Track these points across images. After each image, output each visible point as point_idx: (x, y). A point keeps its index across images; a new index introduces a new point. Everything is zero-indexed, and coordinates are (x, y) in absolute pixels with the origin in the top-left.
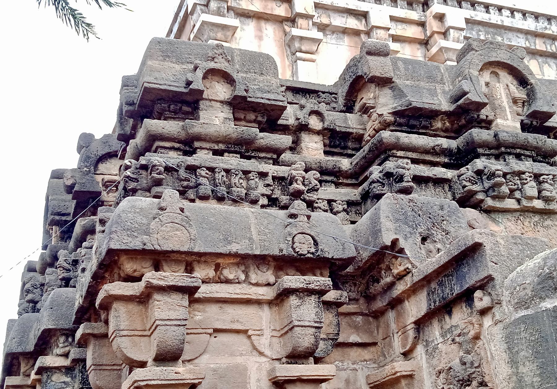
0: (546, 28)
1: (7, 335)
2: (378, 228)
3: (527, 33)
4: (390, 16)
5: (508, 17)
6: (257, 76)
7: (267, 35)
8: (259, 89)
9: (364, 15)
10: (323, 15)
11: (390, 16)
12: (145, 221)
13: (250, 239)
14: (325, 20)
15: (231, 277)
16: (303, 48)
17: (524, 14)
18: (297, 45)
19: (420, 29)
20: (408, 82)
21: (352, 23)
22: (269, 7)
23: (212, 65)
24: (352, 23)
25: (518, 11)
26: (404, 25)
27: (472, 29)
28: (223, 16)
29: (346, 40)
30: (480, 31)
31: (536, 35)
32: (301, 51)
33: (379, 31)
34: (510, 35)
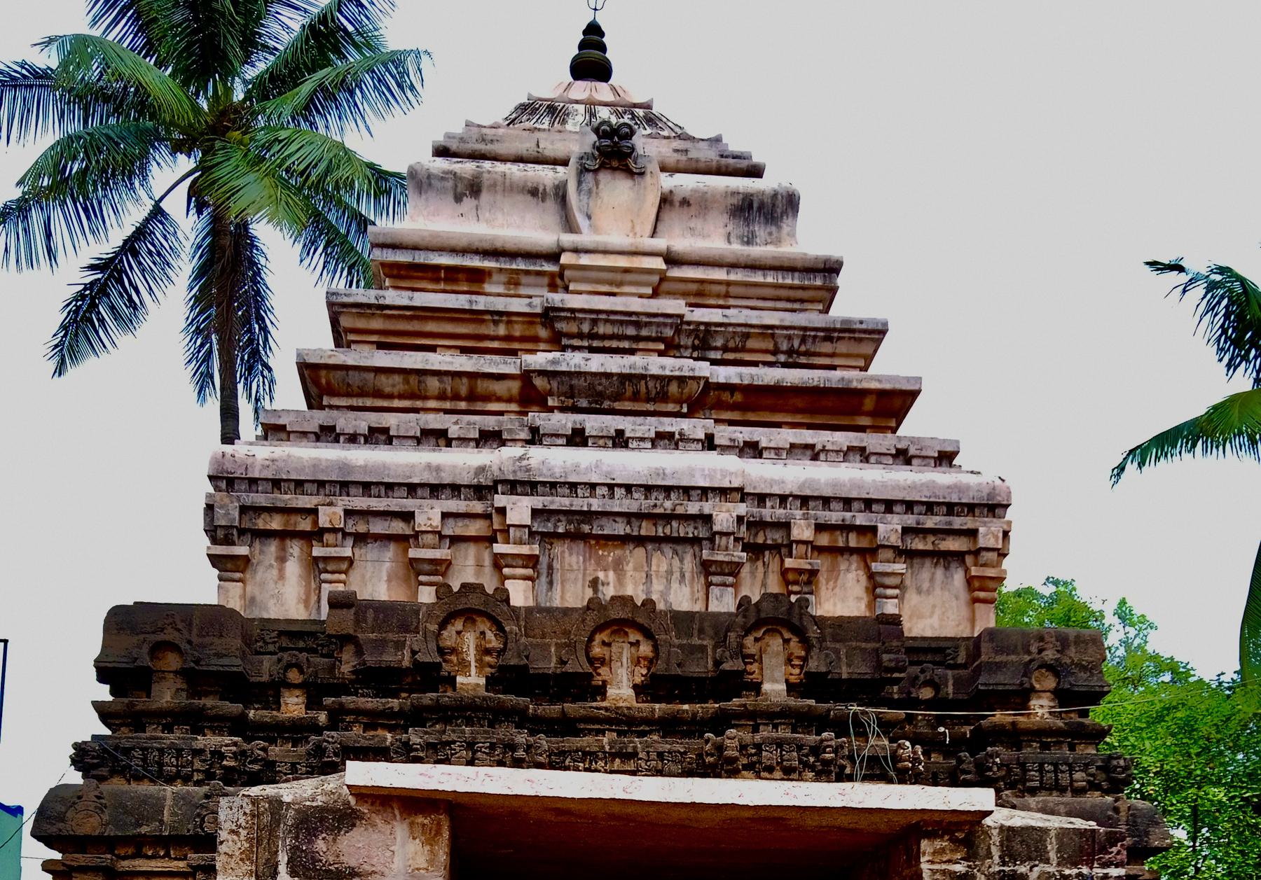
0: (655, 506)
1: (567, 768)
2: (208, 828)
3: (628, 516)
4: (93, 703)
5: (604, 496)
6: (216, 640)
7: (291, 555)
8: (215, 655)
9: (408, 517)
10: (361, 522)
11: (93, 703)
12: (63, 809)
13: (161, 822)
14: (362, 528)
15: (150, 853)
16: (329, 568)
17: (629, 488)
18: (321, 566)
19: (487, 523)
20: (372, 636)
21: (398, 527)
22: (292, 522)
23: (161, 637)
24: (398, 527)
25: (620, 486)
26: (467, 521)
27: (548, 520)
28: (233, 544)
29: (392, 547)
30: (559, 521)
31: (640, 516)
32: (327, 572)
33: (425, 536)
34: (604, 521)
